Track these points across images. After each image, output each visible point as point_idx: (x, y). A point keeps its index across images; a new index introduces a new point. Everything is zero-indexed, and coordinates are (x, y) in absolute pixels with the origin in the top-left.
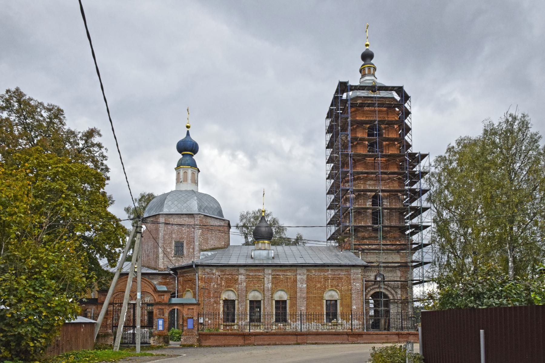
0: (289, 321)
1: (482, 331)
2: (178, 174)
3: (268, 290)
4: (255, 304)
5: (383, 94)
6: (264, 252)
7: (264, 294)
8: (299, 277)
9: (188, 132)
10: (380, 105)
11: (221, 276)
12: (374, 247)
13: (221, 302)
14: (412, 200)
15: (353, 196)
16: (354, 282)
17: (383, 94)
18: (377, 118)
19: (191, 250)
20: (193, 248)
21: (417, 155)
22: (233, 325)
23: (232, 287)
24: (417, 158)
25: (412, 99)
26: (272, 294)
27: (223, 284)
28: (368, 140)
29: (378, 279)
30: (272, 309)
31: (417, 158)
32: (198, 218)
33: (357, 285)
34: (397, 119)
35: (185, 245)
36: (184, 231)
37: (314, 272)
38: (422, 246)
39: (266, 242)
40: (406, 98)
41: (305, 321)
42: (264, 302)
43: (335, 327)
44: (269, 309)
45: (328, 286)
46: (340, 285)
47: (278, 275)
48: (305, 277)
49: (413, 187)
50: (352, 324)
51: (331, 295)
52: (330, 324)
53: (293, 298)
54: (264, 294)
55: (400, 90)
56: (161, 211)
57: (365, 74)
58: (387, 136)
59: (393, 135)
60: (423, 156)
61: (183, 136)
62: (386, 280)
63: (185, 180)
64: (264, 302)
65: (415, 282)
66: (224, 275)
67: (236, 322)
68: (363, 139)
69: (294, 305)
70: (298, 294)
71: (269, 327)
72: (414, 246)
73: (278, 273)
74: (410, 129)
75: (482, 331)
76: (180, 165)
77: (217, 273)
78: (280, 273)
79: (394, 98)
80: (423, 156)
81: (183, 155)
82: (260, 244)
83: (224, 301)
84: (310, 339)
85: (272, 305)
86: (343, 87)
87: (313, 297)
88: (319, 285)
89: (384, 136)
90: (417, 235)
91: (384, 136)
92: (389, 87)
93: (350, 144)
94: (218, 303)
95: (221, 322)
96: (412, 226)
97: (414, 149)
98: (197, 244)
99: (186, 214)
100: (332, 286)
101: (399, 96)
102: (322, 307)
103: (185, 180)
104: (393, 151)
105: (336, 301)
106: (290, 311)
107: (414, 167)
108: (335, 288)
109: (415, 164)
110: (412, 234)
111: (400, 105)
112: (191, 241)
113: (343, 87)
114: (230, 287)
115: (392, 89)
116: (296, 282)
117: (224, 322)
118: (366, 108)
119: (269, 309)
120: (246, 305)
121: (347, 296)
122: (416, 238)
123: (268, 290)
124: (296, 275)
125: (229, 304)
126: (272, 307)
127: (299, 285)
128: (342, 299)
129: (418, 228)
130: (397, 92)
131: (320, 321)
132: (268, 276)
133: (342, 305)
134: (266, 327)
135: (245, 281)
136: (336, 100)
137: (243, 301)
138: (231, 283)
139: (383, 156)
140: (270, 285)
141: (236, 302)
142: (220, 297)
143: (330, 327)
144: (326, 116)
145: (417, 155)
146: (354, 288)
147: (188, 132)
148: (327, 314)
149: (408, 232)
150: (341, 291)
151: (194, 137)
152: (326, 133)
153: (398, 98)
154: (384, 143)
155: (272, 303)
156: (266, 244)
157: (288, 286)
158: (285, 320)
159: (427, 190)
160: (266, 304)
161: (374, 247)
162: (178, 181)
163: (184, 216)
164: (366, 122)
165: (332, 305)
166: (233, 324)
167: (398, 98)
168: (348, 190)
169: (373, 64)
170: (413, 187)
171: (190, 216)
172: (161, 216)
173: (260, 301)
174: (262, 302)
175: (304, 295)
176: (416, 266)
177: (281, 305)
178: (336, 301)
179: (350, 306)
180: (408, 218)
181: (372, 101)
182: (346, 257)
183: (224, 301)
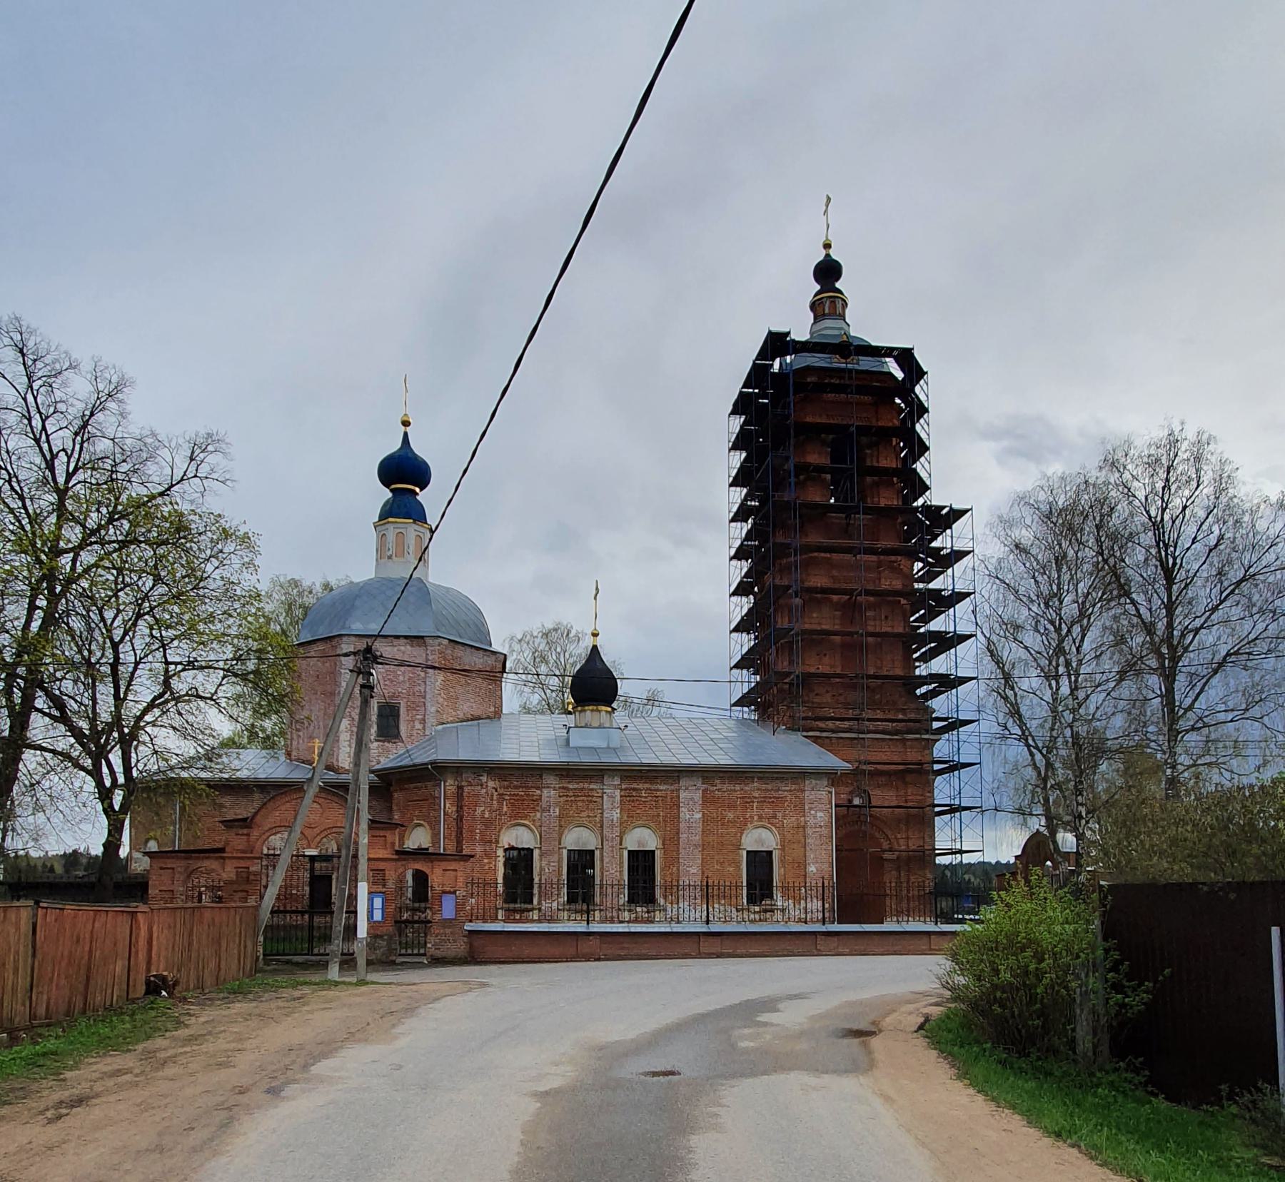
0: (662, 901)
1: (1275, 931)
2: (382, 538)
3: (612, 826)
4: (581, 863)
5: (866, 363)
6: (594, 738)
7: (602, 834)
8: (683, 795)
9: (406, 434)
10: (861, 390)
11: (501, 791)
12: (830, 724)
13: (500, 853)
14: (932, 615)
15: (798, 601)
16: (811, 809)
17: (866, 363)
18: (855, 421)
19: (418, 726)
20: (423, 721)
21: (944, 512)
22: (529, 911)
23: (525, 817)
24: (946, 518)
25: (930, 377)
26: (561, 835)
27: (505, 809)
28: (831, 471)
29: (856, 801)
30: (621, 872)
31: (946, 518)
32: (433, 645)
33: (819, 814)
34: (897, 423)
35: (403, 711)
36: (401, 678)
37: (721, 788)
38: (954, 725)
39: (604, 708)
40: (914, 372)
41: (699, 901)
42: (602, 854)
43: (768, 914)
44: (612, 871)
45: (752, 817)
46: (779, 815)
47: (634, 789)
48: (698, 796)
49: (932, 586)
50: (806, 909)
51: (759, 838)
52: (757, 909)
53: (671, 843)
54: (602, 834)
55: (906, 357)
56: (343, 628)
57: (824, 315)
58: (876, 464)
59: (887, 462)
60: (957, 514)
61: (396, 445)
62: (874, 803)
63: (401, 551)
64: (602, 854)
65: (937, 809)
66: (508, 787)
67: (535, 901)
68: (821, 469)
69: (672, 861)
70: (683, 837)
71: (615, 914)
72: (936, 725)
73: (635, 786)
74: (927, 449)
75: (1275, 931)
76: (388, 512)
77: (491, 784)
78: (641, 786)
79: (890, 374)
80: (957, 514)
81: (392, 491)
82: (588, 713)
83: (506, 850)
84: (706, 946)
85: (621, 863)
86: (776, 343)
87: (718, 840)
88: (730, 815)
89: (869, 464)
90: (943, 696)
91: (869, 464)
92: (883, 348)
93: (792, 480)
94: (491, 855)
95: (499, 902)
96: (933, 677)
97: (936, 497)
98: (432, 709)
99: (406, 637)
100: (760, 818)
101: (903, 370)
102: (739, 868)
103: (401, 551)
104: (887, 499)
105: (770, 853)
106: (663, 877)
107: (935, 538)
108: (769, 820)
109: (937, 531)
110: (934, 694)
111: (906, 388)
112: (418, 704)
113: (776, 343)
114: (521, 818)
115: (889, 352)
116: (679, 807)
117: (505, 901)
118: (831, 396)
119: (612, 871)
120: (560, 861)
121: (795, 838)
122: (940, 705)
123: (612, 826)
124: (678, 790)
125: (520, 862)
126: (621, 867)
127: (685, 814)
128: (783, 849)
129: (947, 683)
130: (897, 362)
131: (734, 899)
132: (611, 794)
133: (783, 862)
134: (609, 915)
135: (557, 804)
136: (758, 375)
137: (551, 853)
138: (521, 811)
139: (867, 511)
140: (616, 814)
141: (536, 853)
142: (497, 842)
143: (757, 916)
144: (731, 408)
145: (944, 512)
146: (811, 822)
147: (406, 434)
148: (750, 885)
149: (923, 690)
150: (781, 829)
151: (420, 448)
152: (730, 450)
153: (900, 375)
154: (869, 479)
155: (621, 856)
156: (603, 713)
157: (658, 815)
158: (651, 900)
159: (969, 594)
160: (606, 860)
161: (846, 724)
162: (382, 553)
163: (402, 641)
164: (828, 428)
165: (760, 862)
166: (529, 906)
167: (900, 375)
168: (789, 587)
169: (840, 292)
170: (932, 586)
171: (415, 642)
172: (345, 639)
173: (592, 852)
174: (597, 853)
175: (697, 838)
176: (941, 772)
177: (641, 863)
178: (770, 853)
179: (802, 865)
180: (917, 659)
181: (840, 378)
182: (789, 749)
183: (506, 850)
